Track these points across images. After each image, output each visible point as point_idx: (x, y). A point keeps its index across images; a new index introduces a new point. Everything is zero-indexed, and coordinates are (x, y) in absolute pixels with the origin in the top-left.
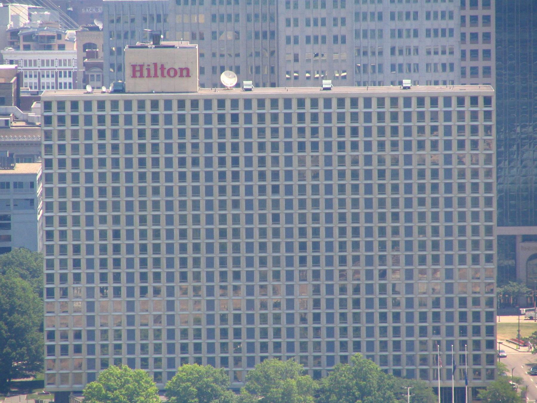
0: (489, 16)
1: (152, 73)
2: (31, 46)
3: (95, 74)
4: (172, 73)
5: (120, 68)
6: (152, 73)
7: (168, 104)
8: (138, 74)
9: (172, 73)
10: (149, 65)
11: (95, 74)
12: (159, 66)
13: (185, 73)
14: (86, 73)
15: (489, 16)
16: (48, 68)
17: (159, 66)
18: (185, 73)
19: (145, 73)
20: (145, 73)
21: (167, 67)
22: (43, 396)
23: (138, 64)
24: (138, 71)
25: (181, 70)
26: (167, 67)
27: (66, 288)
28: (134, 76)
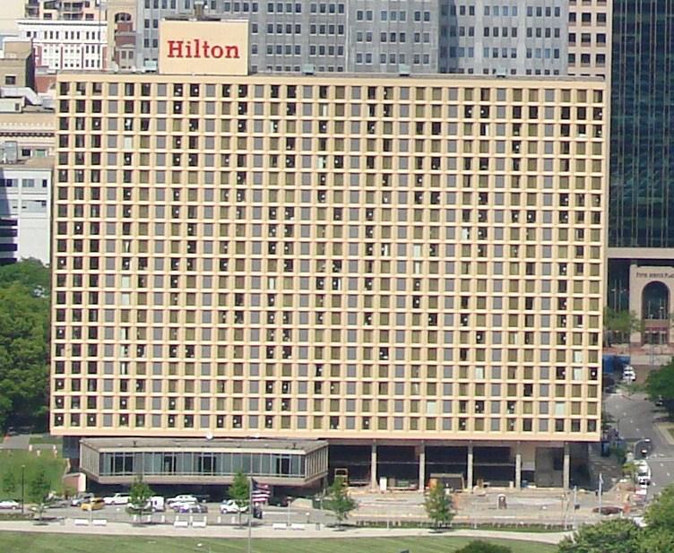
0: (604, 56)
1: (193, 52)
2: (53, 16)
3: (128, 51)
4: (217, 52)
5: (156, 44)
6: (193, 52)
7: (194, 89)
8: (176, 53)
9: (217, 52)
10: (189, 43)
11: (128, 51)
12: (202, 44)
13: (233, 52)
14: (117, 50)
15: (604, 56)
16: (51, 41)
17: (202, 44)
18: (233, 52)
19: (185, 52)
20: (185, 52)
21: (211, 45)
22: (428, 521)
23: (176, 40)
24: (175, 48)
25: (229, 48)
26: (211, 45)
27: (583, 195)
28: (171, 56)
